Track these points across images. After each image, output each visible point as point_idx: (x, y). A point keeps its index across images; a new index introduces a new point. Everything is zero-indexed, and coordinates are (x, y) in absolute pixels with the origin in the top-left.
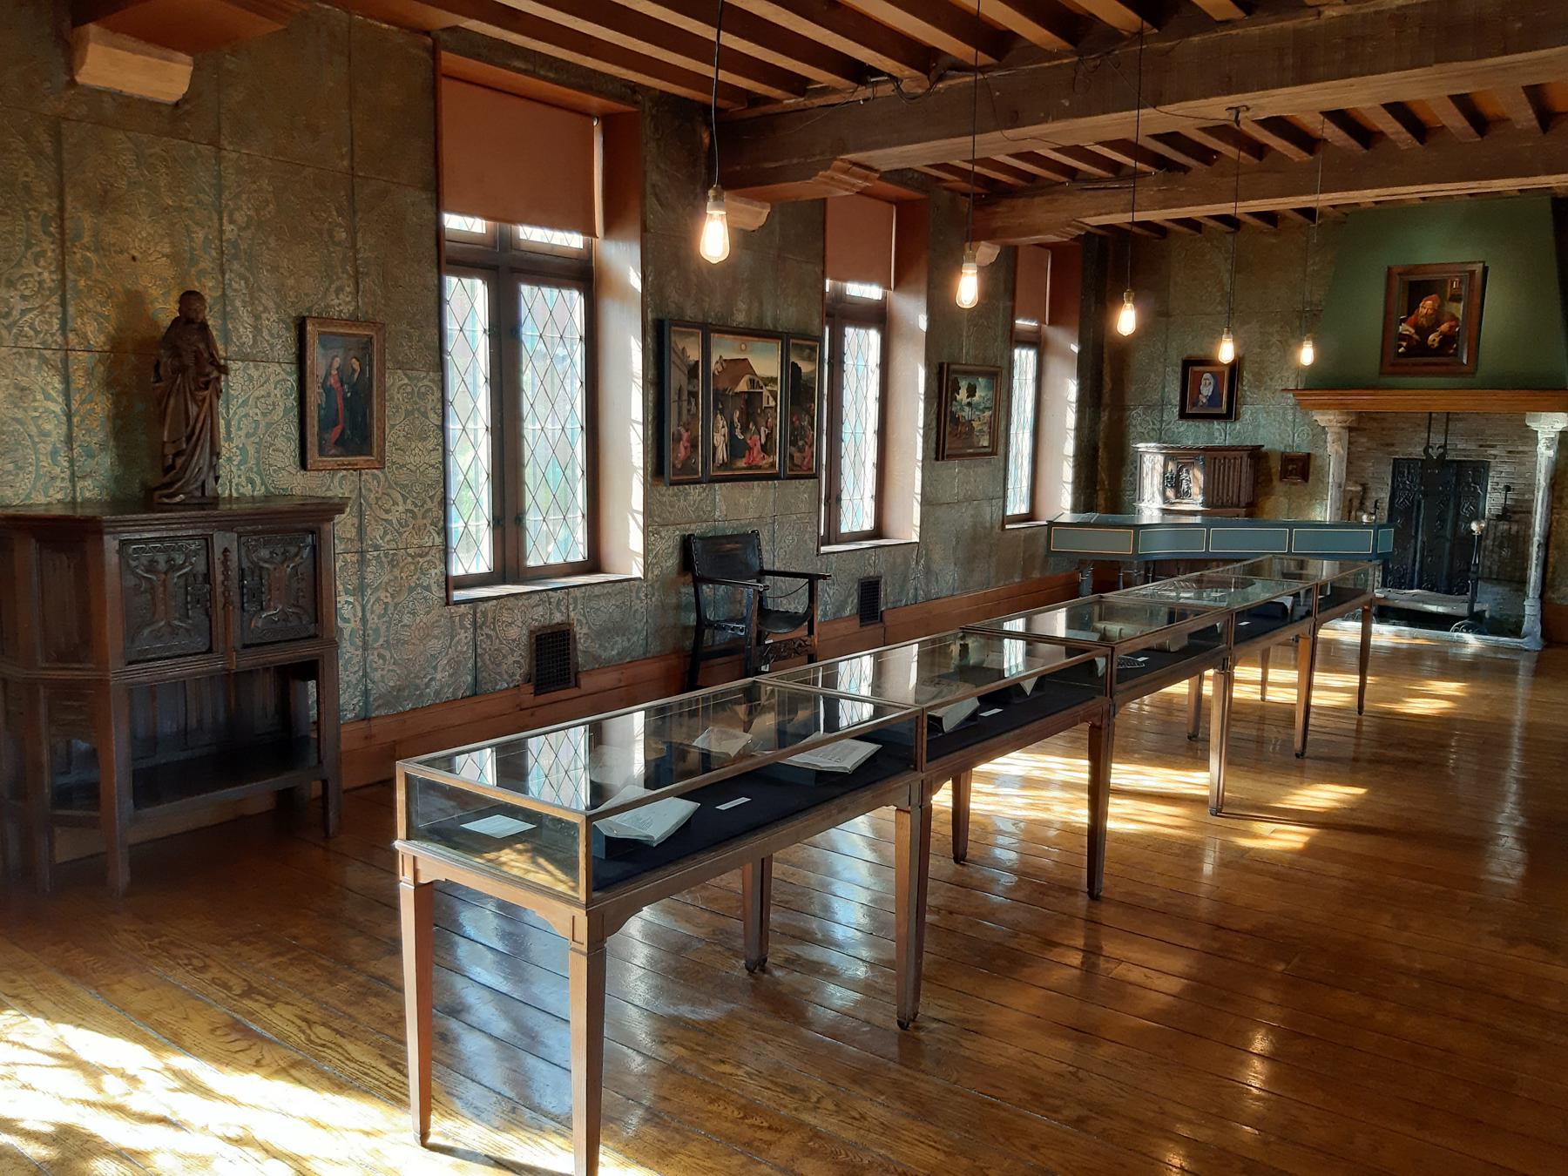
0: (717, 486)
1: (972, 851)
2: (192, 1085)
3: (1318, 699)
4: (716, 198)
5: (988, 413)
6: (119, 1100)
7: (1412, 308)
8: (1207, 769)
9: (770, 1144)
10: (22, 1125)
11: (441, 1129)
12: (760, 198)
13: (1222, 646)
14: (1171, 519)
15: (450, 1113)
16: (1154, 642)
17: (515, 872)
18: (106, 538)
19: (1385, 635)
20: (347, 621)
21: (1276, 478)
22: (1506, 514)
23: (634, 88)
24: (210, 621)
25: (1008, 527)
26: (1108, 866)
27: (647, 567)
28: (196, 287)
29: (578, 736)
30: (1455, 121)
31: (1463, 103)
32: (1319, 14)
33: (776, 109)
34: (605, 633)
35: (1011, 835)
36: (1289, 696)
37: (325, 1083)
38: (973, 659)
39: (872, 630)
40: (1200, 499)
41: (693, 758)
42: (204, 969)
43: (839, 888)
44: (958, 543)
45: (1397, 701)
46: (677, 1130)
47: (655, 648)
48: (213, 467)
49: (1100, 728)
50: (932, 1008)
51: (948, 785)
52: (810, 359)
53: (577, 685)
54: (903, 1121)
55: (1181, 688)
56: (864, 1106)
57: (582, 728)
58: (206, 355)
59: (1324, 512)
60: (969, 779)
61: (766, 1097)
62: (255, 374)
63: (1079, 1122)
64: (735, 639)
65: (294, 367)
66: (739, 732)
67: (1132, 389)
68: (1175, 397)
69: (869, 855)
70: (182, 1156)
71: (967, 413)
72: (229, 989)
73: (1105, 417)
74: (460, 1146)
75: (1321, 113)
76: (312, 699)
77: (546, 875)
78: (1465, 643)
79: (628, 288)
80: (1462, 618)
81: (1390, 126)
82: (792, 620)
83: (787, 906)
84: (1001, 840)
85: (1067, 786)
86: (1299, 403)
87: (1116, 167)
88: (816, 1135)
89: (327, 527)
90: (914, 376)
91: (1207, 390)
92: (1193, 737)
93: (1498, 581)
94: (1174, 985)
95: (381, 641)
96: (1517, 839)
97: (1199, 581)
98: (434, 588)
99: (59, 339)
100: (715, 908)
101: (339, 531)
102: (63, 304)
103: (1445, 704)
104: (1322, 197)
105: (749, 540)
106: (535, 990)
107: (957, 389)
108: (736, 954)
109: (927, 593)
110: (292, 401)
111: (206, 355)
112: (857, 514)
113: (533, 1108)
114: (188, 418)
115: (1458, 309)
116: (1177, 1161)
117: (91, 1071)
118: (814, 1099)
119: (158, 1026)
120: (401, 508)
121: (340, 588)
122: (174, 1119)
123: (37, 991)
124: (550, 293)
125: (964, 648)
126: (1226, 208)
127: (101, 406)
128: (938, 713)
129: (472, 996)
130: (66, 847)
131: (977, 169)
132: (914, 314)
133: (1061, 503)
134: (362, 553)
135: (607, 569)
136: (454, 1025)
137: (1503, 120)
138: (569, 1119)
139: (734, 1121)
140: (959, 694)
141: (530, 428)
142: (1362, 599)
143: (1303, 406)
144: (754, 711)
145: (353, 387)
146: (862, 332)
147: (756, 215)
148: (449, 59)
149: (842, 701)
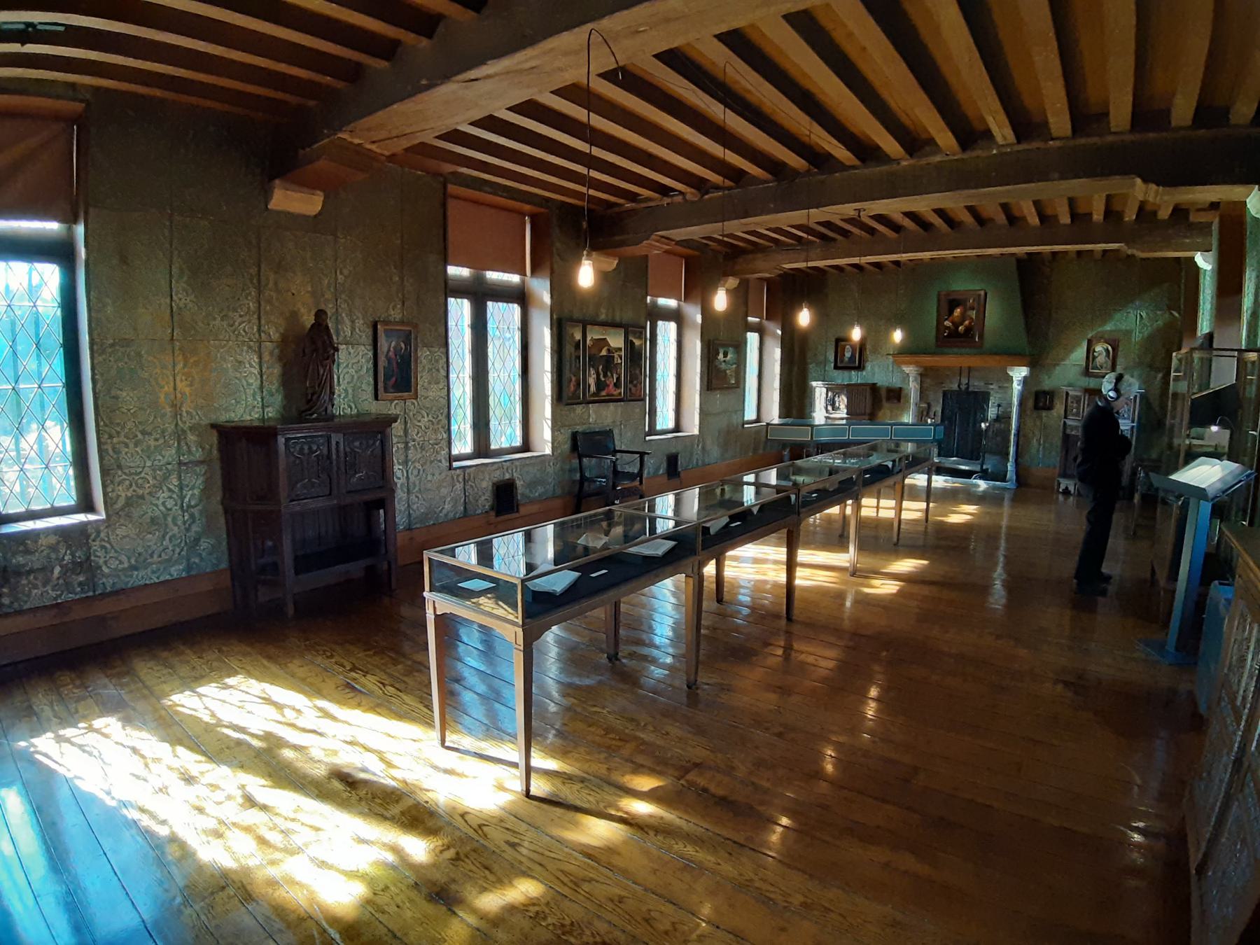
0: (590, 405)
1: (726, 597)
2: (327, 715)
3: (905, 515)
4: (587, 255)
5: (734, 366)
6: (292, 721)
7: (951, 312)
8: (848, 552)
9: (619, 747)
10: (249, 730)
11: (451, 738)
12: (614, 255)
13: (856, 488)
14: (830, 422)
15: (455, 732)
16: (821, 486)
17: (486, 609)
18: (279, 437)
19: (939, 481)
20: (399, 479)
21: (884, 400)
22: (998, 419)
23: (548, 200)
24: (330, 480)
25: (746, 426)
26: (797, 603)
27: (553, 448)
28: (322, 307)
29: (518, 537)
30: (967, 218)
31: (971, 209)
32: (899, 163)
33: (622, 209)
34: (532, 485)
35: (747, 588)
36: (891, 514)
37: (393, 715)
38: (727, 496)
39: (676, 481)
40: (845, 411)
41: (580, 549)
42: (332, 656)
43: (657, 617)
44: (719, 434)
45: (946, 516)
46: (571, 740)
47: (559, 492)
48: (331, 399)
49: (792, 532)
50: (703, 678)
51: (713, 562)
52: (640, 338)
53: (518, 511)
54: (689, 735)
55: (835, 510)
56: (669, 728)
57: (521, 533)
58: (328, 342)
59: (908, 418)
60: (724, 559)
61: (618, 724)
62: (352, 351)
63: (780, 735)
64: (601, 486)
65: (371, 347)
66: (603, 536)
67: (809, 355)
68: (832, 358)
69: (673, 600)
70: (324, 750)
71: (723, 366)
72: (344, 667)
73: (796, 369)
74: (461, 748)
75: (902, 213)
76: (382, 519)
77: (503, 610)
78: (978, 486)
79: (542, 303)
80: (977, 472)
81: (937, 221)
82: (631, 477)
83: (629, 627)
84: (742, 591)
85: (776, 562)
86: (894, 362)
87: (799, 239)
88: (644, 742)
89: (389, 430)
90: (695, 347)
91: (848, 355)
92: (841, 536)
93: (994, 453)
94: (831, 664)
95: (417, 489)
96: (1003, 586)
97: (844, 454)
98: (443, 461)
99: (257, 336)
100: (591, 628)
101: (394, 432)
102: (259, 318)
103: (969, 517)
104: (904, 255)
105: (609, 434)
106: (499, 669)
107: (718, 354)
108: (602, 651)
109: (703, 461)
110: (371, 365)
111: (328, 342)
112: (665, 419)
113: (499, 729)
114: (318, 374)
115: (973, 314)
116: (829, 752)
117: (279, 707)
118: (642, 724)
119: (311, 685)
120: (426, 419)
121: (395, 461)
122: (319, 731)
123: (252, 666)
124: (502, 305)
125: (723, 490)
126: (855, 260)
127: (277, 370)
128: (707, 525)
129: (467, 673)
130: (264, 595)
131: (725, 239)
132: (695, 315)
133: (773, 414)
134: (407, 443)
135: (532, 449)
136: (457, 686)
137: (992, 220)
138: (516, 734)
139: (601, 736)
140: (719, 514)
141: (492, 376)
142: (927, 464)
143: (898, 364)
144: (610, 526)
145: (402, 357)
146: (667, 323)
147: (611, 264)
148: (452, 188)
149: (658, 519)
